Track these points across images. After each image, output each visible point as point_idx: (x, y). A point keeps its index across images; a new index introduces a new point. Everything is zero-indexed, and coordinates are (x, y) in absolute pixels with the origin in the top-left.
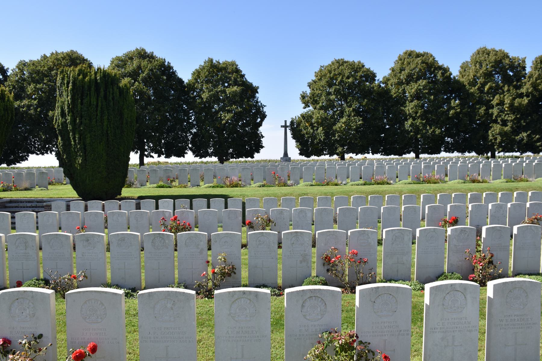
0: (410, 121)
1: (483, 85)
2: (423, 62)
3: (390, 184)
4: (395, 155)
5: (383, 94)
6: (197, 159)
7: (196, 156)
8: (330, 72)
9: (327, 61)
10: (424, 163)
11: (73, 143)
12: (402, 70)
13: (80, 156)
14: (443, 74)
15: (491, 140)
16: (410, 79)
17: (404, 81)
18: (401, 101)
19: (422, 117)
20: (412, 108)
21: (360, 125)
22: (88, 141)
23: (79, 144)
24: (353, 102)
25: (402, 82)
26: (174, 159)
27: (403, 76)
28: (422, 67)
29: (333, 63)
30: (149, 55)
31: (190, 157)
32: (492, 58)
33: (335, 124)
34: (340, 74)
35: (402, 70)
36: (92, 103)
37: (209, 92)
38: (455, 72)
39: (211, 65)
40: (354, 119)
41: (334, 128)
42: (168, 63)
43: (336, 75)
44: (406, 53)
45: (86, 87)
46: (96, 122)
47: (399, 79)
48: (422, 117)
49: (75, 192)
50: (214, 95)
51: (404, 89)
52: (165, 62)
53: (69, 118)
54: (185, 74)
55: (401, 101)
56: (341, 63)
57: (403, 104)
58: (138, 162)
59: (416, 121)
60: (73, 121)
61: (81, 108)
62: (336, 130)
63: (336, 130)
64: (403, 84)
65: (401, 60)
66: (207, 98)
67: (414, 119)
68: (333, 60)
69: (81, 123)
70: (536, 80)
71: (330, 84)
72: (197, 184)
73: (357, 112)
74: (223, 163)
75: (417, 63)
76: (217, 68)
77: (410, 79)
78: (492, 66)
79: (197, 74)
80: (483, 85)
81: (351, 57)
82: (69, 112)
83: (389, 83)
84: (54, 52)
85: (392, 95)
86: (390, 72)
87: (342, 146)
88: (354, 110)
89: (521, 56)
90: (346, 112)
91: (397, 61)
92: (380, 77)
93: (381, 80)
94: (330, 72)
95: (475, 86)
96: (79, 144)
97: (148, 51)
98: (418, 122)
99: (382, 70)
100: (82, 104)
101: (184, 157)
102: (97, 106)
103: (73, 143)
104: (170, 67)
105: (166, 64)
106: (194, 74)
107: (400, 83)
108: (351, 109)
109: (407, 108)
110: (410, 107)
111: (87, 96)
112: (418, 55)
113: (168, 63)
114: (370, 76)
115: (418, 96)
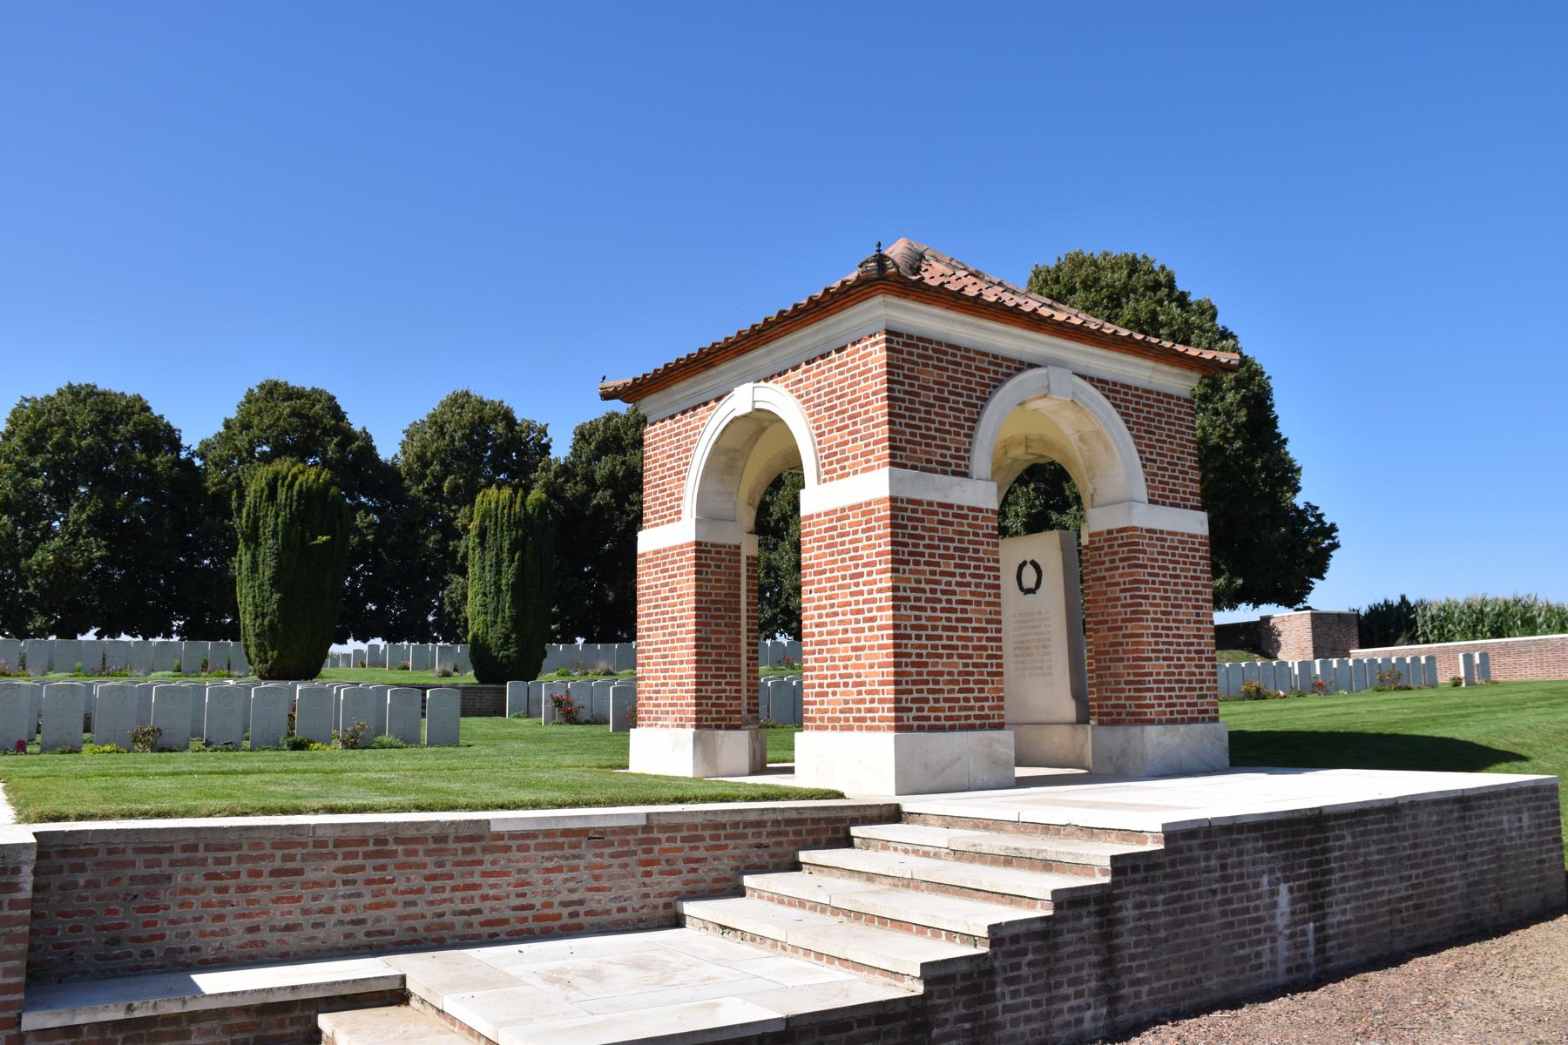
1: (440, 479)
2: (295, 413)
3: (834, 826)
8: (39, 414)
9: (45, 386)
14: (342, 446)
15: (450, 614)
29: (60, 393)
32: (468, 416)
38: (388, 449)
40: (87, 544)
43: (53, 425)
44: (262, 387)
56: (80, 395)
62: (29, 568)
65: (249, 402)
68: (63, 385)
70: (556, 477)
71: (34, 448)
78: (464, 437)
80: (440, 479)
81: (116, 380)
84: (404, 437)
86: (222, 429)
87: (46, 613)
89: (540, 422)
93: (195, 447)
94: (39, 414)
95: (421, 482)
99: (198, 418)
112: (292, 394)
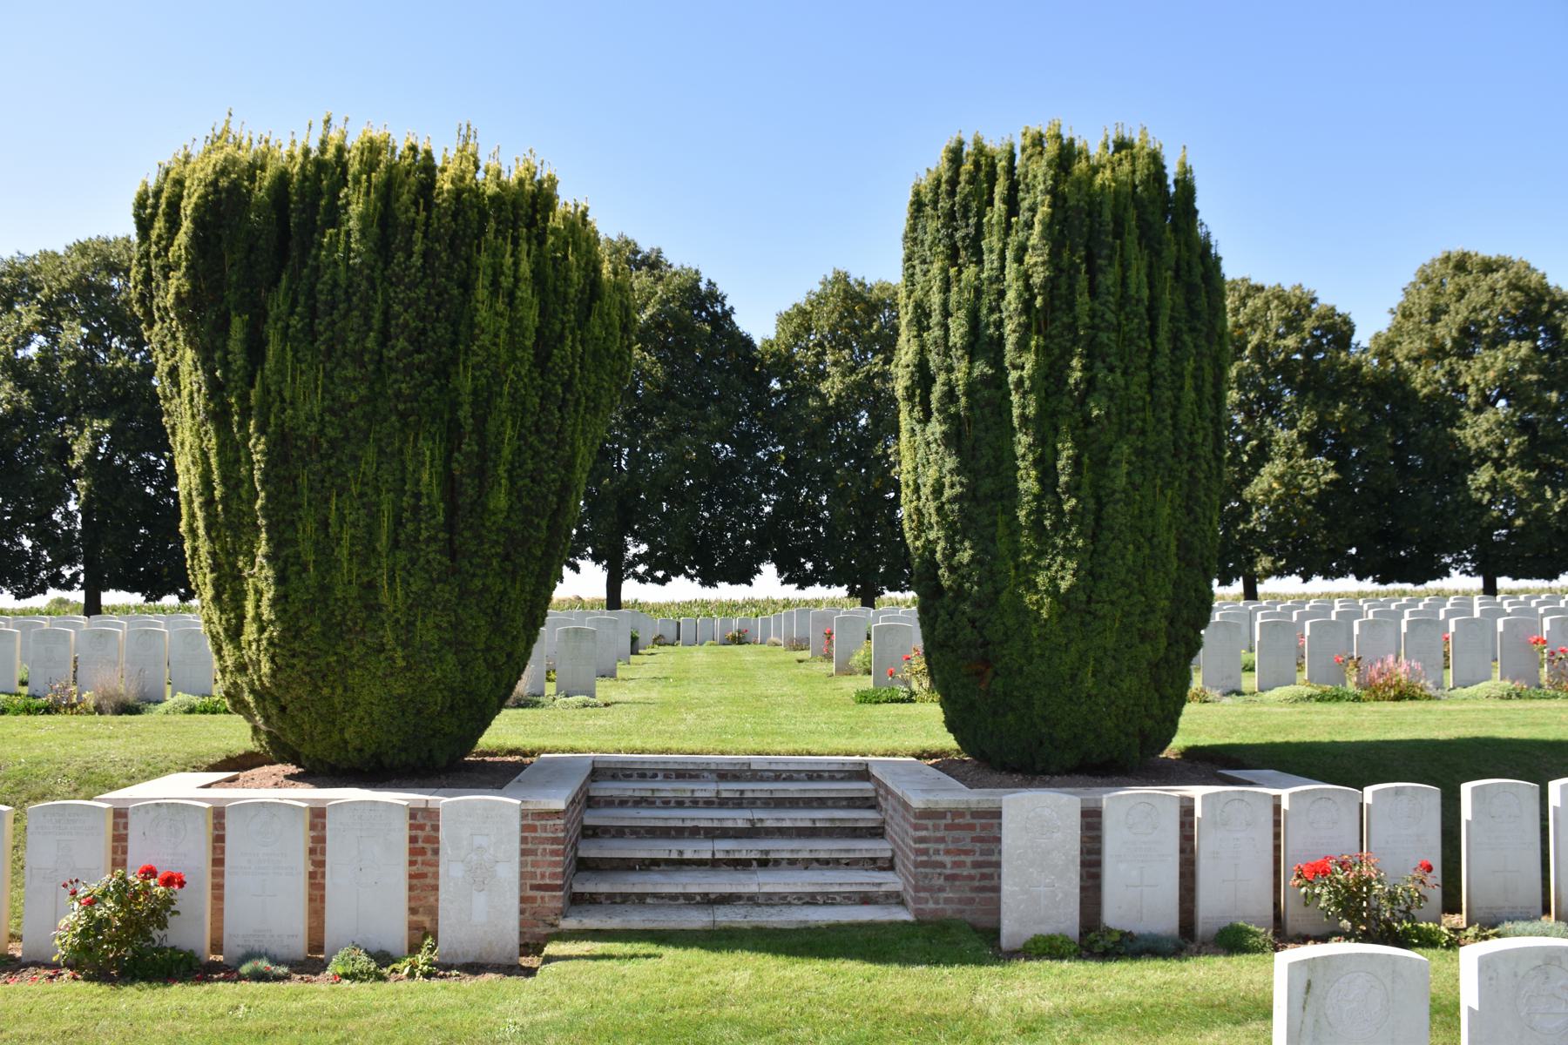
0: (1484, 475)
4: (1401, 581)
5: (1387, 390)
6: (791, 591)
7: (787, 581)
10: (1264, 616)
11: (1028, 483)
12: (1436, 313)
13: (1069, 551)
16: (1468, 340)
17: (1449, 344)
18: (1444, 409)
19: (1526, 459)
20: (1488, 432)
21: (1331, 483)
22: (1120, 478)
23: (1073, 489)
24: (1300, 412)
25: (1442, 348)
26: (726, 592)
27: (1446, 331)
28: (1514, 299)
30: (648, 257)
31: (768, 582)
33: (1246, 481)
34: (1252, 323)
35: (1436, 313)
36: (1132, 292)
37: (844, 375)
39: (845, 291)
41: (1247, 493)
42: (710, 282)
43: (1241, 327)
45: (1107, 215)
46: (1151, 385)
47: (1432, 339)
48: (1526, 459)
49: (952, 736)
50: (858, 386)
51: (1452, 369)
52: (699, 280)
53: (1022, 366)
54: (758, 321)
55: (1444, 409)
57: (1454, 419)
58: (602, 593)
59: (1505, 473)
60: (1050, 378)
61: (1093, 314)
62: (1253, 499)
63: (1253, 499)
64: (1447, 354)
66: (838, 396)
67: (1499, 467)
69: (1090, 382)
72: (1231, 685)
73: (1313, 442)
74: (868, 602)
75: (1492, 289)
76: (863, 299)
77: (1468, 340)
79: (800, 321)
82: (1025, 331)
83: (1399, 353)
85: (1415, 392)
86: (1390, 317)
88: (1302, 436)
90: (1277, 442)
91: (1413, 284)
92: (1363, 337)
96: (1073, 489)
97: (645, 247)
98: (1514, 476)
100: (1093, 292)
101: (750, 584)
102: (1152, 311)
103: (1028, 483)
104: (714, 296)
105: (703, 286)
106: (785, 319)
107: (1437, 352)
108: (1295, 433)
109: (1469, 432)
110: (1476, 431)
111: (1110, 258)
112: (1488, 267)
113: (710, 282)
114: (1339, 331)
115: (1510, 387)
